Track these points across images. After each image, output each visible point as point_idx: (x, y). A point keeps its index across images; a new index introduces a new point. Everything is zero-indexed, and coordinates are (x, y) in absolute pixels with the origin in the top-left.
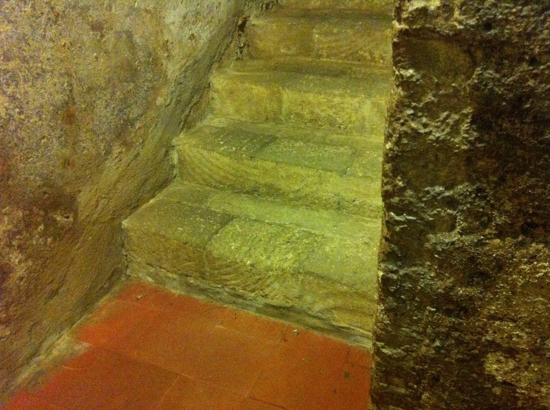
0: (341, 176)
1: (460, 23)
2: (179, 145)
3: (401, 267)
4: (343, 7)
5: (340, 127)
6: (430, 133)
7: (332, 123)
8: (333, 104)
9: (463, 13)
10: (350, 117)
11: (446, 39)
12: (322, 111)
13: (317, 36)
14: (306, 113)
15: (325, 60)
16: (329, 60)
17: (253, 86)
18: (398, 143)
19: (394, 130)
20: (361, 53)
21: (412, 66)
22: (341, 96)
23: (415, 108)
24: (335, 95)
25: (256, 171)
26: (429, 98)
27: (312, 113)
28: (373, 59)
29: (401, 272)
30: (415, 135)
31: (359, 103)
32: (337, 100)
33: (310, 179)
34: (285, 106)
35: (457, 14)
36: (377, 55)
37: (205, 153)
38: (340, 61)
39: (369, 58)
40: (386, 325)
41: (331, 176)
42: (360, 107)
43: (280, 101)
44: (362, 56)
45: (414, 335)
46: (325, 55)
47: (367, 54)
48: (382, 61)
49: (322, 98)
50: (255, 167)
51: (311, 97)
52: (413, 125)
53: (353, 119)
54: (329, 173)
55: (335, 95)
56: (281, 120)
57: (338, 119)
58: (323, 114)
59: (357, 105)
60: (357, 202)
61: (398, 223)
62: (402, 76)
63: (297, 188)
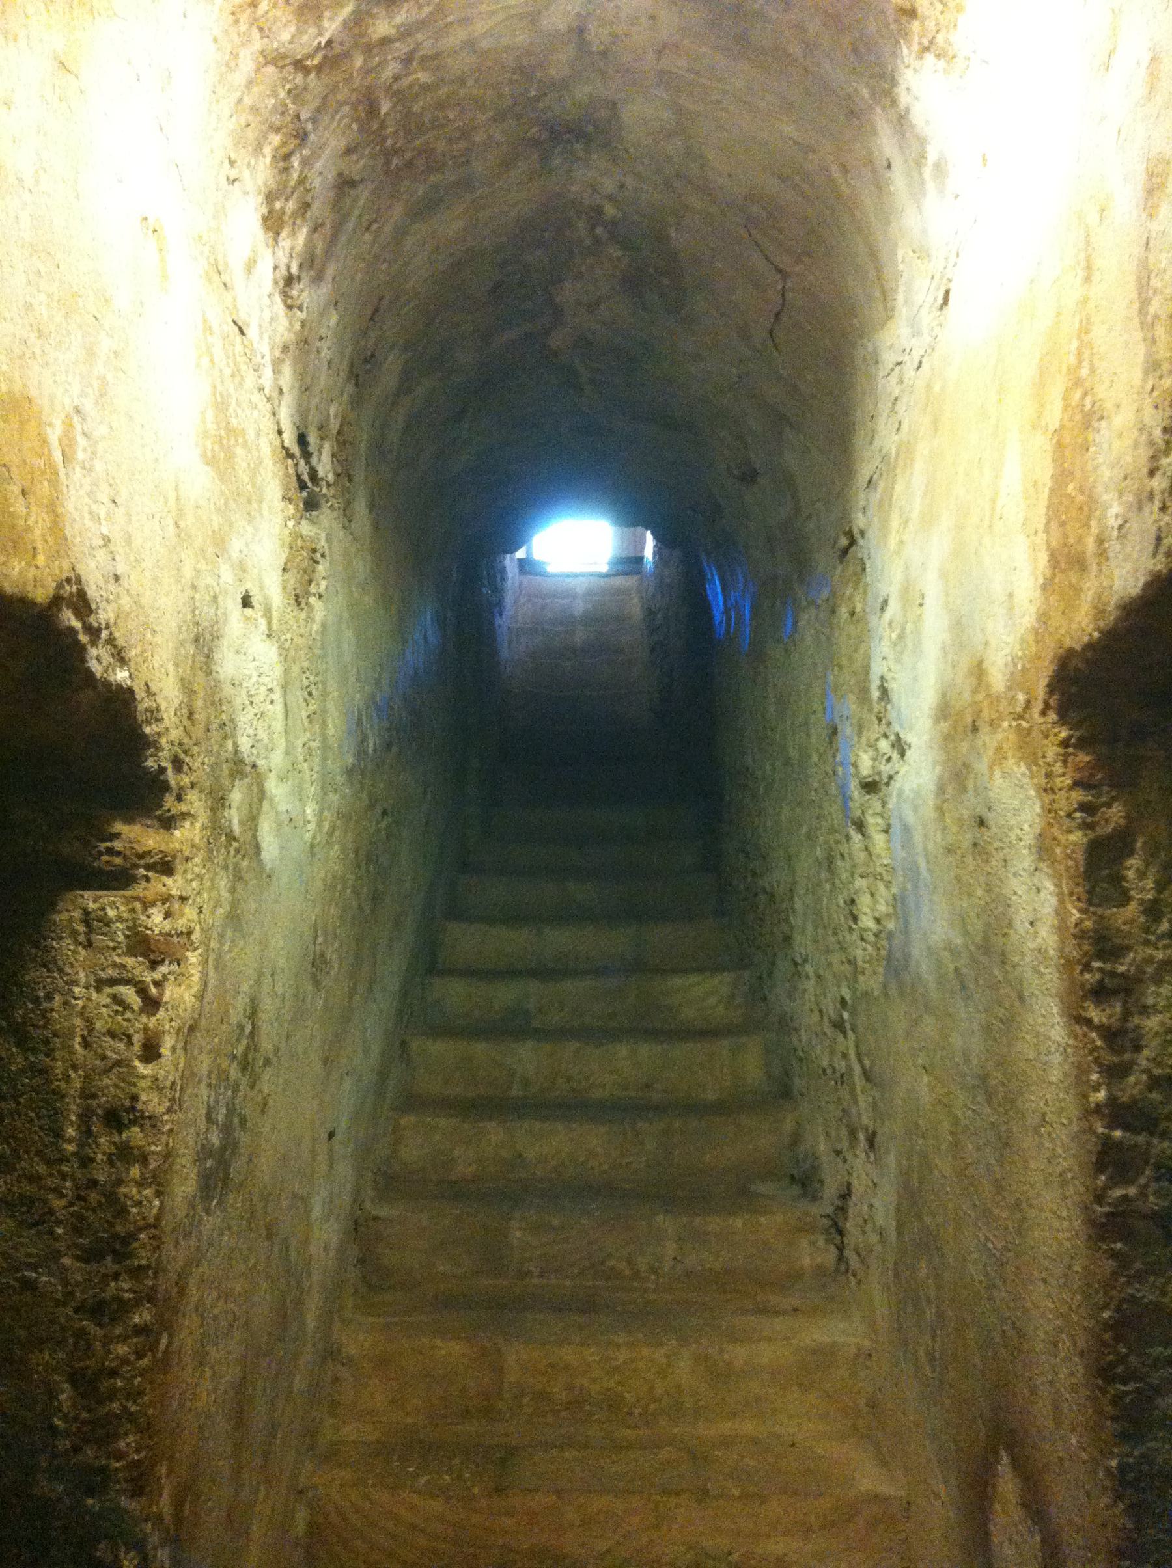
0: (699, 1501)
1: (1157, 1205)
2: (315, 1487)
3: (1135, 1447)
4: (523, 1175)
5: (630, 1413)
6: (1144, 1297)
7: (613, 1404)
8: (614, 1363)
9: (1157, 1198)
10: (652, 1389)
11: (1145, 1217)
12: (594, 1380)
13: (518, 1234)
14: (559, 1393)
15: (535, 1281)
16: (544, 1281)
17: (439, 1343)
18: (1118, 1309)
19: (1111, 1298)
20: (612, 1262)
21: (1121, 1240)
22: (630, 1345)
23: (1127, 1276)
24: (618, 1346)
25: (508, 1522)
26: (1138, 1265)
27: (570, 1388)
28: (636, 1275)
29: (1136, 1453)
30: (1132, 1299)
31: (668, 1357)
32: (622, 1356)
33: (635, 1520)
34: (511, 1378)
35: (1151, 1198)
36: (642, 1264)
37: (382, 1496)
38: (568, 1283)
39: (628, 1272)
40: (1130, 1531)
41: (678, 1506)
42: (669, 1365)
43: (499, 1370)
44: (613, 1268)
45: (1161, 1536)
46: (536, 1271)
47: (622, 1265)
48: (653, 1277)
49: (591, 1354)
50: (510, 1513)
51: (568, 1354)
52: (1130, 1291)
53: (659, 1392)
54: (674, 1500)
55: (618, 1346)
56: (500, 1412)
57: (626, 1395)
58: (595, 1388)
59: (664, 1361)
60: (735, 1557)
61: (1126, 1393)
62: (1112, 1249)
63: (602, 1545)
